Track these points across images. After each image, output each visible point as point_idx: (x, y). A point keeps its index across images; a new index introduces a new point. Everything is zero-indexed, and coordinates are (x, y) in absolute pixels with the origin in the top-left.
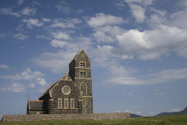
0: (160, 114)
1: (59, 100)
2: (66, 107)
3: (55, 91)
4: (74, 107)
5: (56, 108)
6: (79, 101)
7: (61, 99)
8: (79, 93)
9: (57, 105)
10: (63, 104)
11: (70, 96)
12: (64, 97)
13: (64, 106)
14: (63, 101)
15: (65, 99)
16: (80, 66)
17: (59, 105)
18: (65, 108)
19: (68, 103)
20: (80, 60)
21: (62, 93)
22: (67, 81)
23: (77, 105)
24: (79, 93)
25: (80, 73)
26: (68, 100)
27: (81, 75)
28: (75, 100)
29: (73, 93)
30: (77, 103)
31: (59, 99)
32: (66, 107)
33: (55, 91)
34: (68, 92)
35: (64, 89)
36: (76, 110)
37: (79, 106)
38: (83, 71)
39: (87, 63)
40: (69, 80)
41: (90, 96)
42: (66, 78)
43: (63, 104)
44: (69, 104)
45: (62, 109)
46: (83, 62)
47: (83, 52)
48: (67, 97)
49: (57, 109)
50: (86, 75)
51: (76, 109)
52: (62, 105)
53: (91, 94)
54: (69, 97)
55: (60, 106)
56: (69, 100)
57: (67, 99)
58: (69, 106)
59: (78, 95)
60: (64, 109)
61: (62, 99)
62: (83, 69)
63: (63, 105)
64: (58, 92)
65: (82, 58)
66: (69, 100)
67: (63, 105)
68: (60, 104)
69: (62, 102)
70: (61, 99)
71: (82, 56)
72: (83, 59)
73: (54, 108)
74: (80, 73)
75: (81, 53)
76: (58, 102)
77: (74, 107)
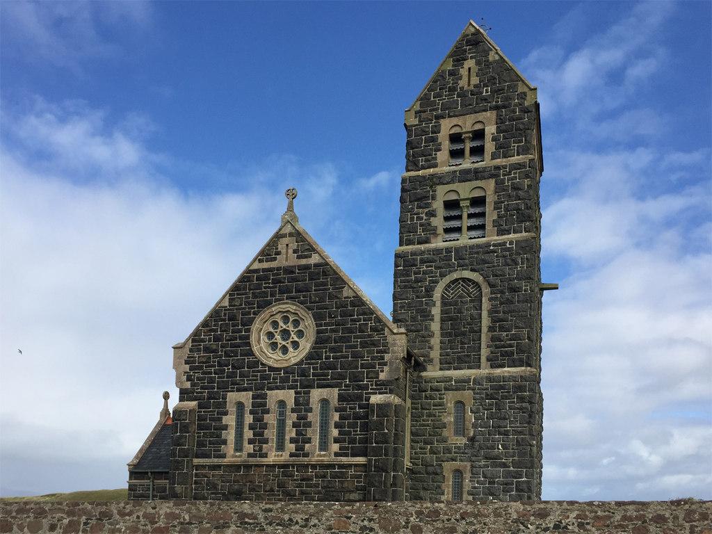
0: (96, 492)
1: (232, 409)
2: (280, 447)
3: (207, 349)
4: (335, 447)
5: (208, 456)
6: (368, 406)
7: (246, 398)
8: (374, 344)
9: (219, 436)
10: (259, 427)
11: (303, 373)
12: (265, 379)
13: (266, 442)
14: (260, 408)
15: (274, 396)
16: (443, 156)
17: (231, 436)
18: (273, 457)
19: (289, 423)
20: (449, 111)
21: (251, 353)
22: (290, 270)
23: (358, 434)
24: (374, 344)
25: (438, 205)
26: (291, 403)
27: (474, 222)
28: (341, 398)
29: (333, 350)
30: (357, 417)
31: (232, 397)
32: (280, 447)
33: (207, 349)
34: (274, 346)
35: (302, 342)
36: (352, 472)
37: (365, 441)
38: (465, 191)
39: (500, 121)
40: (304, 262)
41: (520, 363)
42: (281, 247)
43: (259, 427)
44: (302, 425)
45: (248, 467)
46: (467, 124)
47: (475, 41)
48: (285, 377)
49: (218, 467)
50: (491, 215)
51: (344, 460)
52: (248, 434)
53: (520, 351)
54: (300, 378)
55: (239, 448)
56: (302, 406)
57: (289, 396)
58: (301, 440)
59: (368, 359)
60: (265, 461)
61: (254, 398)
62: (465, 176)
63: (259, 438)
64: (227, 355)
65: (462, 95)
66: (302, 406)
67: (259, 438)
68: (239, 434)
69: (249, 419)
70: (246, 398)
71: (463, 83)
72: (473, 101)
73: (196, 461)
74: (438, 205)
75: (458, 57)
76: (230, 420)
77: (335, 447)
